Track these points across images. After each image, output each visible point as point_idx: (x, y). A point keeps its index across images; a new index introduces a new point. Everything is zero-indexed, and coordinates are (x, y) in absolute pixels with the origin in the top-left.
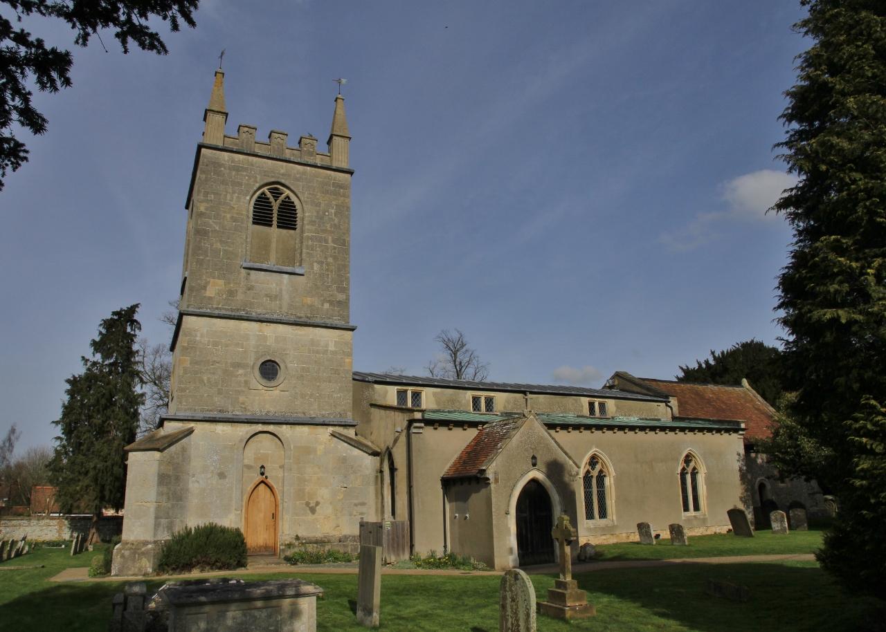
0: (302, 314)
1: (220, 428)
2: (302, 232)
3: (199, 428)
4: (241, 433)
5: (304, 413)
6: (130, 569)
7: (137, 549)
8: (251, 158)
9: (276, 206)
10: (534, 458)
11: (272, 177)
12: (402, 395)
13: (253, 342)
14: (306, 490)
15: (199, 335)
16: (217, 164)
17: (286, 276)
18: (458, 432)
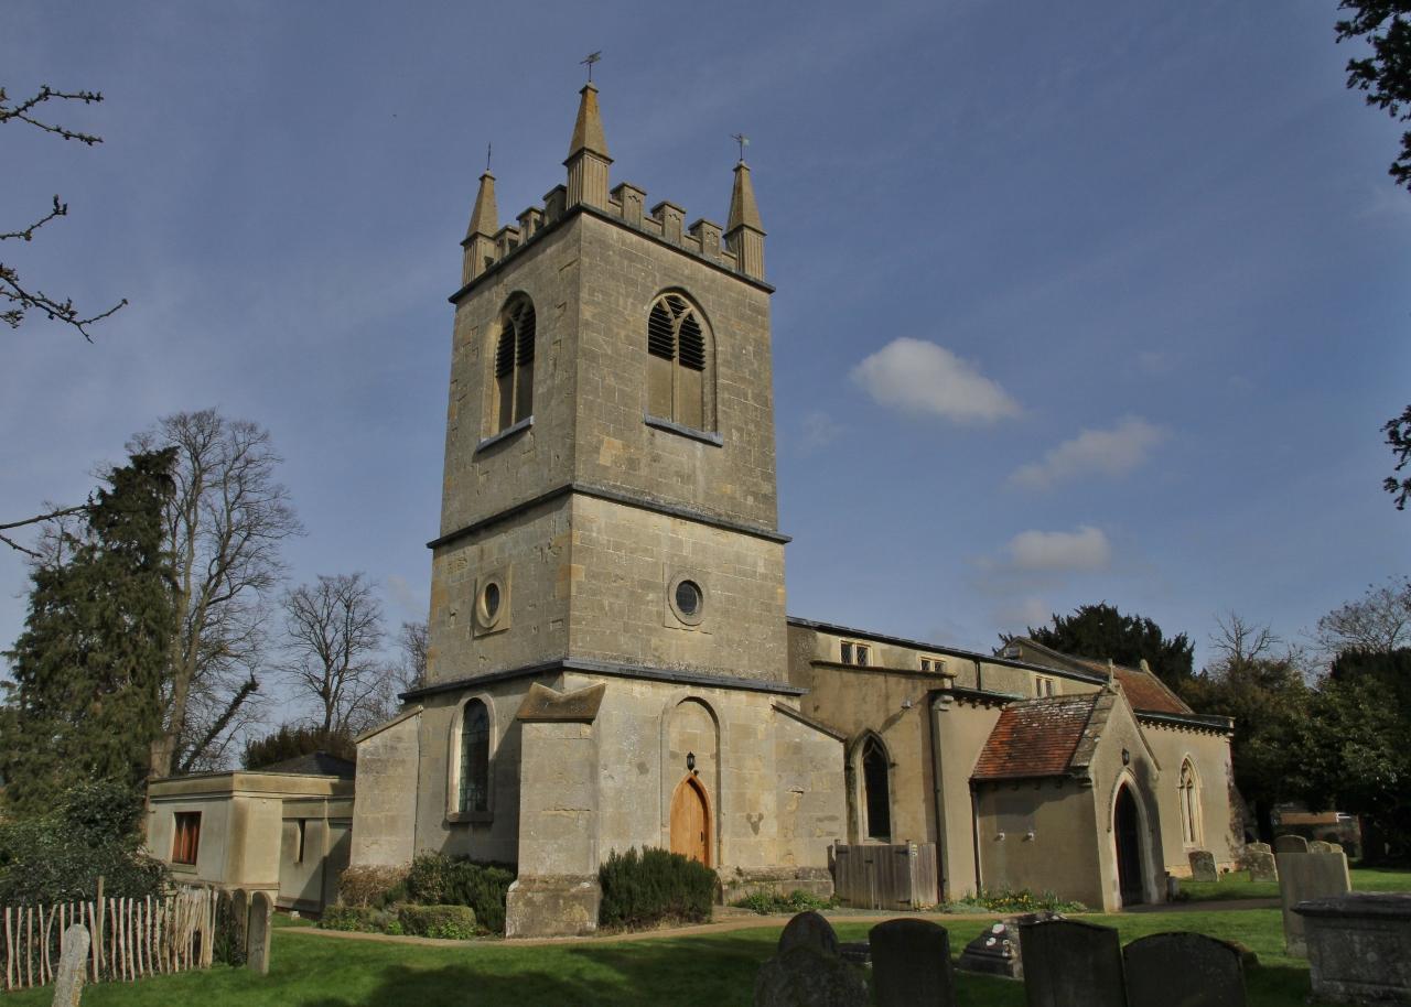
0: (723, 510)
3: (613, 687)
6: (547, 925)
7: (558, 892)
8: (647, 243)
10: (1125, 752)
11: (675, 279)
12: (846, 649)
15: (595, 529)
17: (699, 445)
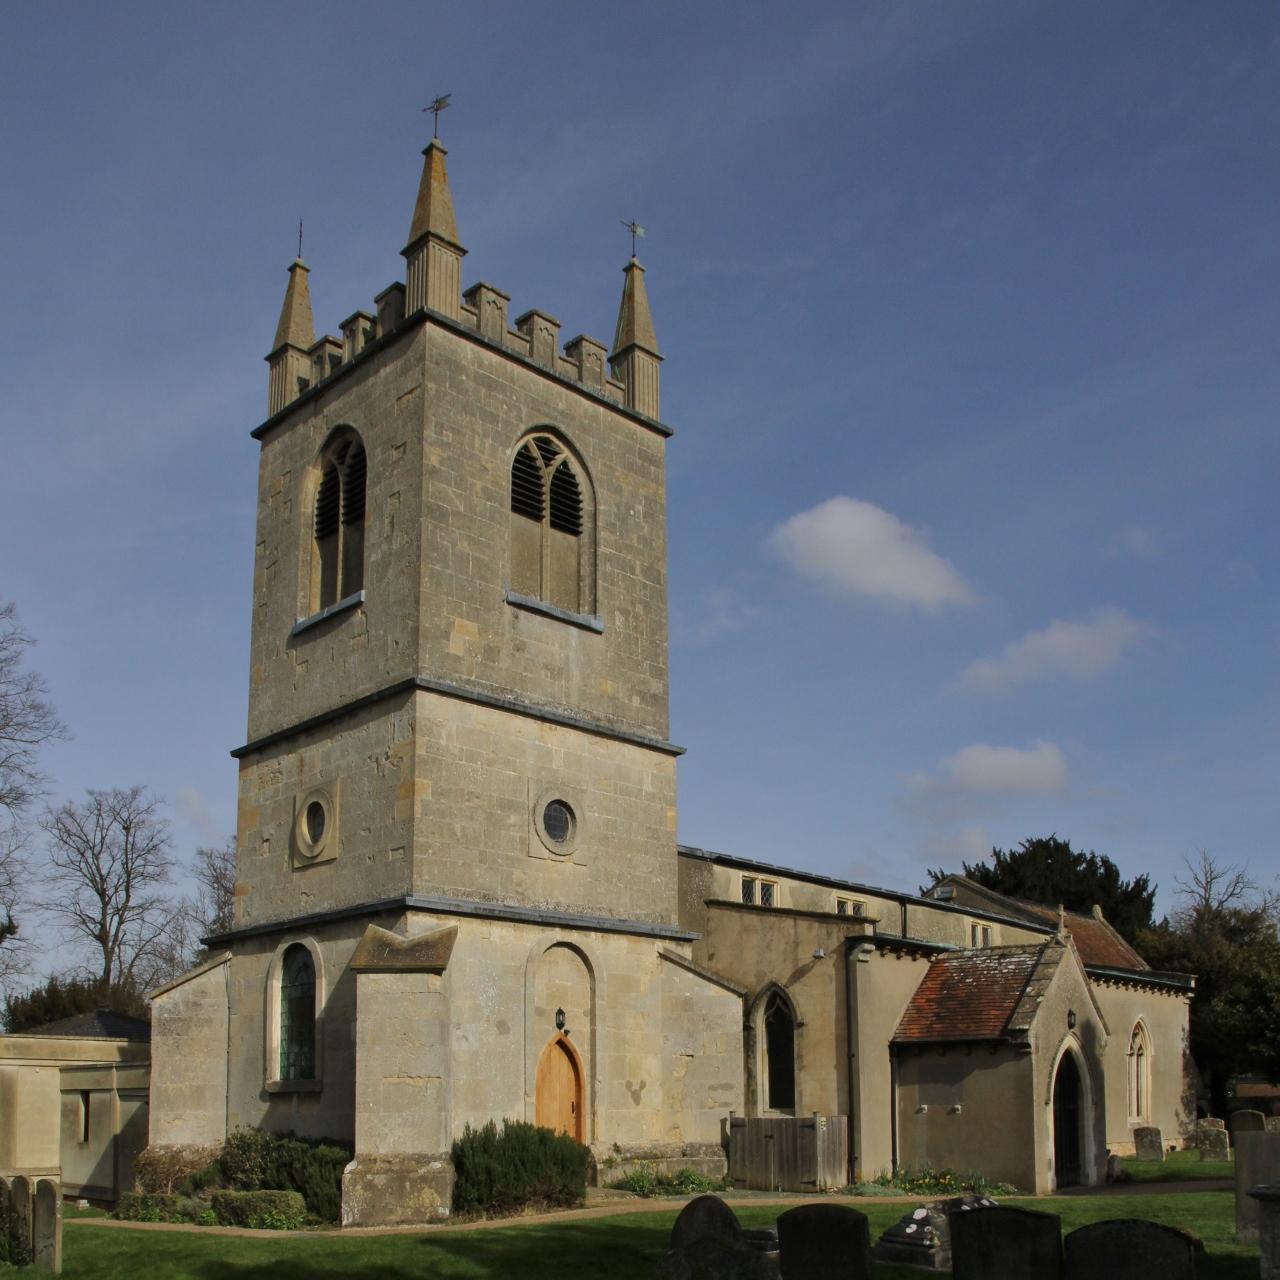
3: (467, 929)
4: (529, 945)
5: (610, 911)
6: (391, 1212)
7: (403, 1174)
8: (510, 365)
9: (547, 475)
10: (1071, 1014)
11: (546, 415)
14: (627, 1060)
15: (444, 735)
17: (574, 631)
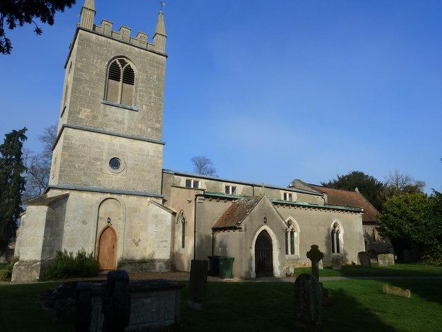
0: (135, 134)
1: (85, 195)
2: (137, 87)
3: (73, 195)
9: (122, 70)
13: (106, 147)
16: (89, 41)
18: (222, 203)
